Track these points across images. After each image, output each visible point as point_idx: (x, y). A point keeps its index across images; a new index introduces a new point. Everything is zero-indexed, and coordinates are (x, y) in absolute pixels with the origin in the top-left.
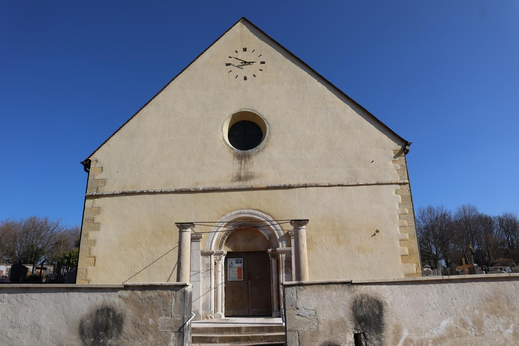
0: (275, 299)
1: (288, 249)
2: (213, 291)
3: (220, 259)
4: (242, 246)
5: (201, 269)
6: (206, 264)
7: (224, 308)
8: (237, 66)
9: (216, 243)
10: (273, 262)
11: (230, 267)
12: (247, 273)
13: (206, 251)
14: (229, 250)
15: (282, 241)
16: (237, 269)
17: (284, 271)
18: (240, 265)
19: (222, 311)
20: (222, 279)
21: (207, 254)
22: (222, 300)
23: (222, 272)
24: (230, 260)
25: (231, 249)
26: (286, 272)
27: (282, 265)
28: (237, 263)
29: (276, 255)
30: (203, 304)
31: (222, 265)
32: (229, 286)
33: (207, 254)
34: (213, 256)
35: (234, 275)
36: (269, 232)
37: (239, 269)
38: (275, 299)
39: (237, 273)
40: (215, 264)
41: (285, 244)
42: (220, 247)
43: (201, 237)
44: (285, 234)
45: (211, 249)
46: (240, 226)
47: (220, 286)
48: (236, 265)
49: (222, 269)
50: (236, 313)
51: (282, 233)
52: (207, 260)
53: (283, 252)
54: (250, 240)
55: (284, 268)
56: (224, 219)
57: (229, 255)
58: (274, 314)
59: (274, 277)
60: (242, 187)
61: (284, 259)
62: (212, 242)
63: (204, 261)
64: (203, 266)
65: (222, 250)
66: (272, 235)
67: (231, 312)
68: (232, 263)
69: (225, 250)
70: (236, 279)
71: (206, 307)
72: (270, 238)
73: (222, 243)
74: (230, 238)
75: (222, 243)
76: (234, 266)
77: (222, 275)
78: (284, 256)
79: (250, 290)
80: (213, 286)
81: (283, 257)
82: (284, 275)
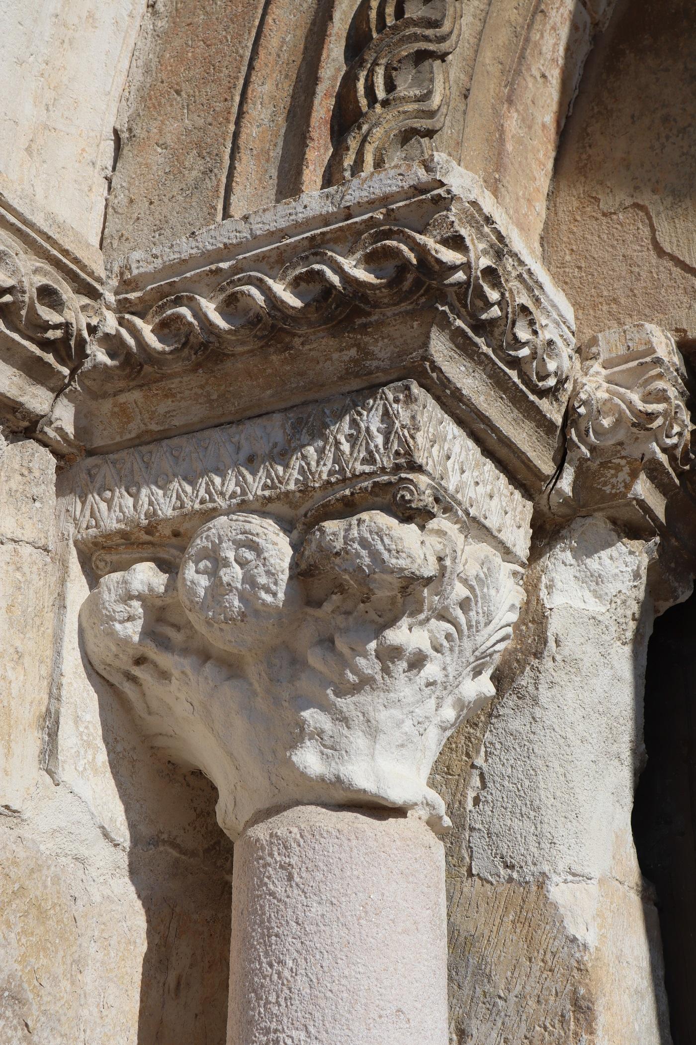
3: (341, 610)
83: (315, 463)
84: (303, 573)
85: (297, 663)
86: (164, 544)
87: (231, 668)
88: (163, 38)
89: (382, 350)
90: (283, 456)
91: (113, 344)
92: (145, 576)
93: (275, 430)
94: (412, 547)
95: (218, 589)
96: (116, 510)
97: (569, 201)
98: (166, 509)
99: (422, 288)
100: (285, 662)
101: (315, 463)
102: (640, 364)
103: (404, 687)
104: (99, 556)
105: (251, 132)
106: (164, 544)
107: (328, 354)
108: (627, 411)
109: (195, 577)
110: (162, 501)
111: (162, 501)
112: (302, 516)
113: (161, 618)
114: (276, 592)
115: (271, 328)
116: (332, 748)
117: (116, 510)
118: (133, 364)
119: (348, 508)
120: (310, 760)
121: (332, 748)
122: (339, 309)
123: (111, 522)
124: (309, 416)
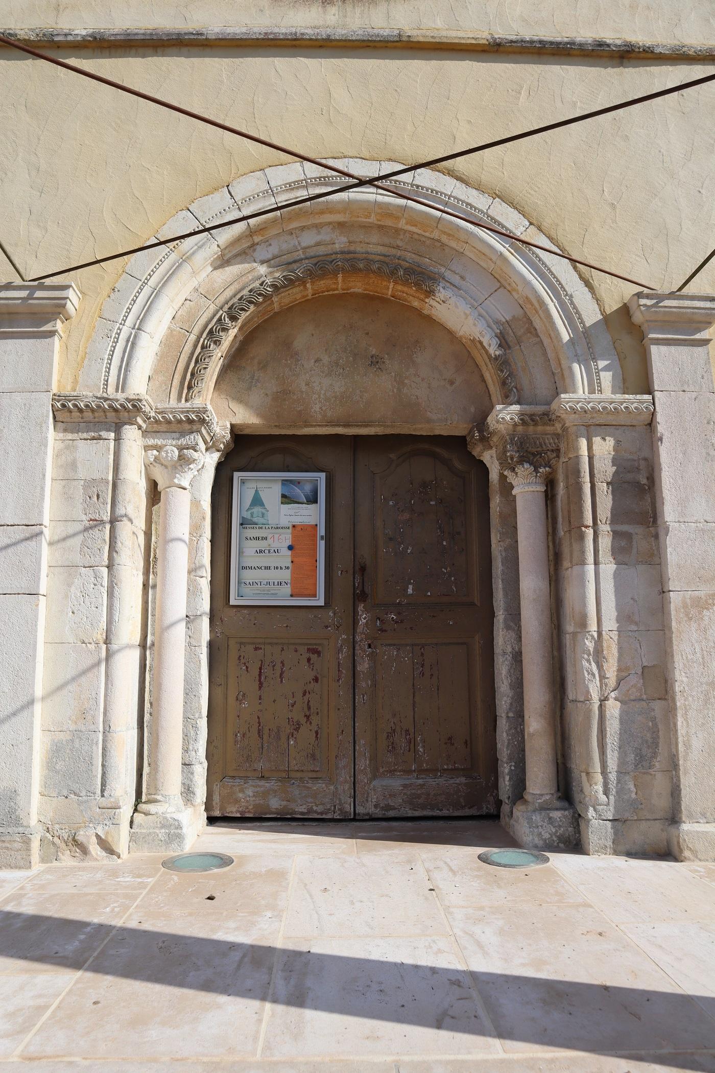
0: (536, 724)
1: (636, 401)
2: (127, 665)
3: (184, 461)
4: (327, 391)
5: (48, 512)
6: (90, 483)
7: (200, 771)
8: (270, 974)
9: (162, 357)
10: (526, 488)
11: (243, 523)
12: (352, 571)
13: (88, 393)
14: (245, 416)
15: (588, 356)
16: (287, 539)
17: (606, 542)
18: (312, 515)
19: (188, 791)
20: (193, 590)
21: (93, 417)
22: (188, 720)
23: (193, 550)
24: (246, 486)
25: (259, 415)
26: (623, 549)
27: (599, 504)
28: (286, 499)
29: (543, 448)
30: (56, 752)
31: (195, 503)
32: (240, 641)
33: (93, 417)
34: (131, 434)
35: (270, 572)
36: (503, 311)
37: (301, 536)
38: (536, 724)
39: (286, 557)
40: (154, 494)
41: (607, 378)
42: (190, 384)
43: (57, 310)
44: (607, 320)
45: (122, 385)
46: (322, 267)
47: (178, 636)
48: (283, 512)
49: (195, 529)
50: (275, 804)
51: (591, 315)
52: (93, 455)
53: (596, 423)
54: (375, 362)
55: (605, 528)
56: (216, 207)
57: (244, 452)
58: (525, 822)
59: (531, 584)
60: (339, 33)
61: (606, 469)
62: (132, 343)
63: (73, 465)
64: (67, 497)
65: (197, 402)
66: (522, 330)
67: (247, 796)
68: (257, 501)
69: (225, 414)
70: (283, 597)
71: (76, 768)
72: (503, 343)
73: (199, 359)
74: (256, 336)
75: (199, 359)
76: (272, 519)
77: (193, 571)
78: (604, 447)
79: (363, 666)
80: (129, 630)
81: (599, 454)
82: (609, 568)
83: (183, 441)
84: (179, 456)
85: (176, 468)
86: (158, 448)
87: (166, 467)
88: (159, 361)
89: (195, 428)
90: (178, 439)
91: (154, 418)
92: (155, 452)
93: (177, 435)
94: (195, 455)
95: (167, 456)
96: (151, 442)
97: (216, 394)
98: (159, 443)
99: (203, 421)
100: (174, 467)
101: (183, 441)
102: (224, 427)
103: (190, 472)
104: (147, 448)
105: (174, 383)
106: (158, 448)
107: (187, 427)
108: (431, 782)
109: (164, 454)
110: (159, 442)
111: (159, 442)
112: (181, 449)
113: (156, 459)
114: (176, 458)
115: (180, 422)
116: (179, 480)
117: (151, 442)
118: (157, 422)
119: (187, 449)
120: (176, 481)
121: (179, 480)
122: (190, 421)
123: (150, 443)
124: (183, 434)
